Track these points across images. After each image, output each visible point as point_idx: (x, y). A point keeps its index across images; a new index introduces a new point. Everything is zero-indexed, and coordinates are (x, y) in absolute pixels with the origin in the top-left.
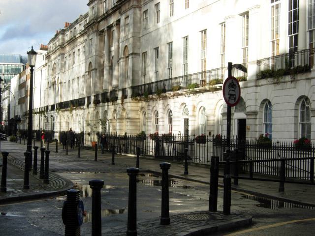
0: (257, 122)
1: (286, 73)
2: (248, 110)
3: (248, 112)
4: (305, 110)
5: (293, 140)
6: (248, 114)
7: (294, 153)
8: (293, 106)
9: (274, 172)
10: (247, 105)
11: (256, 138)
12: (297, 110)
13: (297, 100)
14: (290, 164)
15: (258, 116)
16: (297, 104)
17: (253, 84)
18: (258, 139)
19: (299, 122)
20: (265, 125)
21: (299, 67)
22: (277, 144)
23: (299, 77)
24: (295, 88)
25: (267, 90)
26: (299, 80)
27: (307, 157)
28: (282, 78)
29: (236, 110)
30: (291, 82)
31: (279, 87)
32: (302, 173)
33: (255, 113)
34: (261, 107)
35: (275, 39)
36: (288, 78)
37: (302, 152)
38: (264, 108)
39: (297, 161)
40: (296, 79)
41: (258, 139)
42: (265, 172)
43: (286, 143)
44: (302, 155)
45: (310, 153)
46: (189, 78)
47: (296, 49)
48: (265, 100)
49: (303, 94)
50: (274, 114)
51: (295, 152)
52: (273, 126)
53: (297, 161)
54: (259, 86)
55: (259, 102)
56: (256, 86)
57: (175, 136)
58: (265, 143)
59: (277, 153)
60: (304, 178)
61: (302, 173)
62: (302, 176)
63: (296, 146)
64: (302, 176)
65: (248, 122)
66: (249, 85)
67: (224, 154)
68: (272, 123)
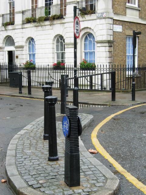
0: (24, 52)
1: (46, 19)
2: (16, 44)
3: (16, 46)
4: (31, 46)
5: (52, 64)
6: (16, 47)
7: (52, 72)
8: (51, 41)
9: (39, 85)
10: (15, 41)
11: (23, 64)
12: (54, 44)
13: (26, 40)
14: (57, 81)
15: (24, 49)
16: (54, 40)
17: (20, 27)
18: (25, 64)
19: (55, 51)
20: (28, 55)
21: (55, 16)
22: (48, 66)
23: (56, 22)
24: (52, 29)
25: (31, 30)
26: (56, 24)
27: (86, 75)
28: (43, 23)
29: (6, 44)
30: (51, 25)
31: (40, 28)
32: (33, 83)
33: (22, 47)
34: (26, 42)
35: (11, 1)
36: (47, 23)
37: (56, 71)
38: (28, 43)
39: (71, 80)
40: (54, 23)
41: (25, 64)
42: (36, 85)
43: (69, 66)
44: (18, 71)
45: (35, 71)
46: (66, 4)
47: (36, 6)
48: (29, 38)
49: (59, 34)
50: (37, 47)
51: (53, 71)
52: (36, 55)
53: (71, 80)
54: (25, 28)
55: (25, 39)
56: (23, 28)
57: (38, 67)
58: (30, 67)
59: (48, 73)
60: (37, 86)
61: (33, 83)
62: (35, 85)
63: (54, 67)
64: (35, 85)
65: (16, 53)
66: (17, 27)
67: (133, 84)
68: (36, 53)
